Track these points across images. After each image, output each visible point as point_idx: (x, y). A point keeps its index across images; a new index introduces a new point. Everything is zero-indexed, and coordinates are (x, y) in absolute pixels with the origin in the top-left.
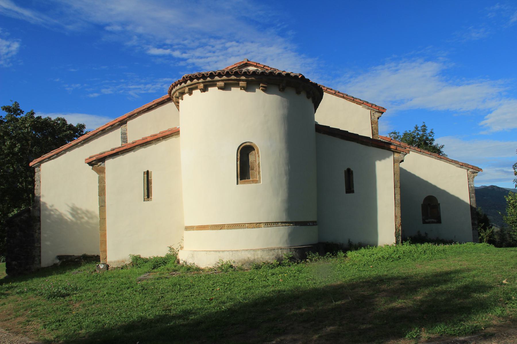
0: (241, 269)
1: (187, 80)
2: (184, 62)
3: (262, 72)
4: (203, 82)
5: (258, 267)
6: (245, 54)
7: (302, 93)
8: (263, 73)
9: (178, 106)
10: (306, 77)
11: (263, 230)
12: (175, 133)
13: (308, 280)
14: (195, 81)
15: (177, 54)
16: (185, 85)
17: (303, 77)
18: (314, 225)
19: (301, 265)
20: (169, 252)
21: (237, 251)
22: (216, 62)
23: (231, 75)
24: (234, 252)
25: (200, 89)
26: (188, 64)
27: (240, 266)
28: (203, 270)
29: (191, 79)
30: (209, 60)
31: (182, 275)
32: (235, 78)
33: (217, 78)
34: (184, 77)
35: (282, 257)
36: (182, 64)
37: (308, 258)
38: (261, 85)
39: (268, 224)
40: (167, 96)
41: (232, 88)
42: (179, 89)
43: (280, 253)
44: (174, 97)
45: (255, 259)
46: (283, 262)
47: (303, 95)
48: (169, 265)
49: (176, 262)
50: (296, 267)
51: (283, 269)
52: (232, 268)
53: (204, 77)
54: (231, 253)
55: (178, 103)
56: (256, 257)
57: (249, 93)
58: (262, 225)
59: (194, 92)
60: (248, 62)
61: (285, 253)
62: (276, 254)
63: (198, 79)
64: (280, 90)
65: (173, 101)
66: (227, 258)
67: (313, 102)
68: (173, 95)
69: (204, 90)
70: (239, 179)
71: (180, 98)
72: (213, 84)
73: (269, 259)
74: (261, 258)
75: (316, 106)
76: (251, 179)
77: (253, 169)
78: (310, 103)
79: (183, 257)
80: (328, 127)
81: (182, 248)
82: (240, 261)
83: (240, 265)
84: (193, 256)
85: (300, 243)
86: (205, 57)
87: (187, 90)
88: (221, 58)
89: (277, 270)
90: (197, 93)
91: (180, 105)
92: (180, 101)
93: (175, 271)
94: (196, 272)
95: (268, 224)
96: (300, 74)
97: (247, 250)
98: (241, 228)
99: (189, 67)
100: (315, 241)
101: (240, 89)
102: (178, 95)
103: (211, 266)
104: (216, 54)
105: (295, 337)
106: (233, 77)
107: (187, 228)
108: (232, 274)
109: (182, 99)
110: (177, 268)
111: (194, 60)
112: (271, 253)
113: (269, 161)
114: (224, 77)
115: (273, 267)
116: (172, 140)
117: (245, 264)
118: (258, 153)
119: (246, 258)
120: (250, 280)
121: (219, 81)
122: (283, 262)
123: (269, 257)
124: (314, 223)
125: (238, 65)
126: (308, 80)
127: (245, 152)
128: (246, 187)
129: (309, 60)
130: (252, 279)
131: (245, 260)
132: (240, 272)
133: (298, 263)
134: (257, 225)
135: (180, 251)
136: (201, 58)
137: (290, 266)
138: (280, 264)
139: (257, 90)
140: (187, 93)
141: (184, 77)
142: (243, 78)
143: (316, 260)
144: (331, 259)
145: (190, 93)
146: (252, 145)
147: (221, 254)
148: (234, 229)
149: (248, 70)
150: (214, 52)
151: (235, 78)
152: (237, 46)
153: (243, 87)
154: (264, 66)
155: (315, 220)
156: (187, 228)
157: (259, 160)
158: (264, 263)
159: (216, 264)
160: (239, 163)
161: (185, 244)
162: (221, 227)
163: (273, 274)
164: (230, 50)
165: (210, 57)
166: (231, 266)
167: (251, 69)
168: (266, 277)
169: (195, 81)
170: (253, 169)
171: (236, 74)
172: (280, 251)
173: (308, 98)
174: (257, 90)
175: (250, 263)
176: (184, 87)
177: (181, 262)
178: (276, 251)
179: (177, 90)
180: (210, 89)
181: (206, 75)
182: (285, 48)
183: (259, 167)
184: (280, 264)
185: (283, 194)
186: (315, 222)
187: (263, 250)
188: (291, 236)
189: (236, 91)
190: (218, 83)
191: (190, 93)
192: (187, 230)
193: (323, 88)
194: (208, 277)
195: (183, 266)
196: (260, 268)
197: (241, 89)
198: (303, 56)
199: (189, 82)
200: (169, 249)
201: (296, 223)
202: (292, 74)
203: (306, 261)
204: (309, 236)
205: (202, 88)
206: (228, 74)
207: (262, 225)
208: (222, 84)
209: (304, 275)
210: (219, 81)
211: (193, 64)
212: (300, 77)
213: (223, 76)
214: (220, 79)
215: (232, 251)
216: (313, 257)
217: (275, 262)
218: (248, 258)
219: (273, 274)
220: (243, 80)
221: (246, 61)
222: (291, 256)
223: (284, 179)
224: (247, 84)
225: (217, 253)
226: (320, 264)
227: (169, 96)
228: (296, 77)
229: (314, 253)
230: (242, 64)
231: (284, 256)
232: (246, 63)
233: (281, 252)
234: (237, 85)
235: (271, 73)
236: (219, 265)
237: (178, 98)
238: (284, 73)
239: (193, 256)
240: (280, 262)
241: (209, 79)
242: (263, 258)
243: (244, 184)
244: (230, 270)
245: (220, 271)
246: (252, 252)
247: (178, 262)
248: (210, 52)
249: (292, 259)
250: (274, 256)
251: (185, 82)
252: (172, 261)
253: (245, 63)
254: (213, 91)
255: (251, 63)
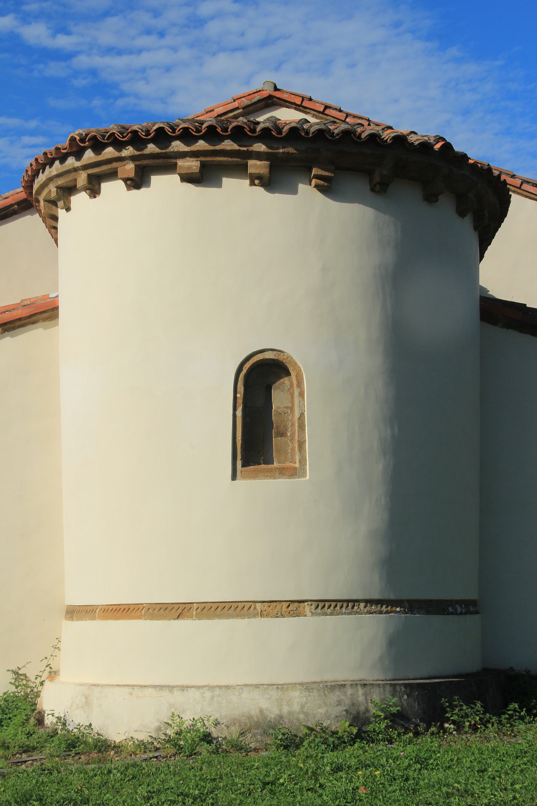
0: (239, 748)
1: (84, 149)
2: (63, 64)
3: (320, 132)
4: (133, 158)
5: (290, 743)
6: (264, 44)
7: (442, 198)
8: (321, 133)
9: (53, 229)
10: (457, 148)
11: (310, 623)
12: (45, 313)
13: (448, 795)
14: (110, 152)
15: (36, 33)
16: (78, 164)
17: (448, 146)
18: (468, 613)
19: (428, 741)
20: (13, 689)
21: (227, 687)
22: (168, 69)
23: (222, 139)
24: (217, 692)
25: (125, 180)
26: (77, 74)
27: (235, 736)
28: (117, 748)
29: (98, 145)
30: (145, 59)
31: (49, 765)
32: (236, 147)
33: (177, 146)
34: (73, 139)
35: (367, 710)
36: (54, 69)
37: (447, 720)
38: (315, 171)
39: (324, 605)
40: (17, 193)
41: (226, 181)
42: (59, 176)
43: (361, 699)
44: (41, 198)
45: (281, 717)
46: (370, 728)
47: (446, 206)
48: (11, 730)
49: (32, 721)
50: (409, 748)
51: (372, 751)
52: (210, 742)
53: (136, 139)
54: (208, 694)
55: (55, 218)
56: (285, 709)
57: (277, 195)
58: (307, 608)
59: (106, 187)
60: (277, 94)
61: (376, 698)
62: (348, 702)
63: (119, 145)
64: (373, 190)
65: (39, 211)
66: (194, 711)
67: (476, 228)
68: (39, 192)
69: (137, 182)
70: (239, 463)
71: (60, 203)
72: (166, 165)
73: (327, 716)
74: (302, 711)
75: (485, 240)
76: (276, 464)
77: (282, 434)
78: (465, 229)
79: (57, 703)
80: (522, 307)
81: (53, 674)
82: (234, 722)
83: (234, 732)
84: (87, 703)
85: (426, 667)
86: (130, 52)
87: (82, 179)
88: (185, 54)
89: (350, 754)
90: (113, 189)
91: (61, 225)
92: (61, 213)
93: (27, 749)
94: (94, 755)
95: (324, 605)
96: (440, 139)
97: (257, 686)
98: (242, 616)
99: (81, 82)
100: (471, 664)
101: (248, 182)
102: (53, 194)
103: (143, 736)
104: (168, 40)
105: (292, 464)
106: (228, 145)
107: (74, 612)
108: (209, 763)
109: (68, 209)
110: (33, 742)
111: (98, 61)
112: (333, 697)
113: (332, 410)
114: (201, 145)
115: (338, 742)
116: (32, 337)
117: (249, 730)
118: (300, 384)
119: (255, 712)
120: (265, 784)
121: (183, 155)
122: (370, 728)
123: (326, 712)
124: (469, 607)
125: (245, 102)
126: (464, 157)
127: (261, 381)
128: (260, 488)
129: (471, 69)
130: (273, 783)
131: (250, 717)
132: (235, 756)
133: (417, 734)
134: (293, 607)
135: (47, 683)
136: (120, 52)
137: (390, 742)
138: (359, 736)
139: (302, 187)
140: (85, 189)
141: (73, 139)
142: (260, 147)
143: (474, 728)
144: (522, 727)
145: (94, 191)
146: (281, 358)
147: (178, 697)
148: (220, 617)
149: (275, 121)
150: (162, 34)
151: (236, 147)
152: (237, 15)
153: (259, 177)
154: (327, 107)
155: (473, 596)
156: (74, 612)
157: (302, 407)
158: (311, 729)
159: (159, 729)
160: (239, 413)
161: (65, 663)
162: (179, 611)
163: (338, 769)
164: (213, 29)
165: (148, 50)
166: (207, 738)
167: (287, 116)
168: (315, 775)
169: (110, 152)
170: (282, 434)
171: (238, 134)
172: (361, 691)
173: (461, 213)
174: (302, 187)
175: (267, 727)
176: (75, 170)
177: (49, 720)
178: (349, 691)
179: (50, 180)
180: (156, 180)
181: (142, 134)
182: (397, 25)
183: (302, 427)
184: (359, 736)
185: (371, 514)
186: (474, 603)
187: (307, 687)
188: (397, 646)
189: (234, 187)
190: (180, 163)
191: (94, 191)
192: (71, 618)
193: (509, 180)
194: (134, 773)
195: (55, 733)
196: (297, 747)
197: (252, 184)
198: (454, 51)
199: (89, 156)
200: (10, 677)
201: (412, 606)
202: (412, 139)
203: (442, 727)
204: (451, 648)
205: (132, 175)
206: (212, 134)
207: (307, 608)
208: (191, 165)
209: (436, 775)
210: (183, 155)
211: (93, 72)
212: (437, 147)
213: (196, 139)
214: (186, 149)
215: (211, 688)
216: (467, 716)
217: (343, 726)
218: (261, 711)
219: (338, 769)
220: (259, 156)
221: (269, 91)
222: (394, 710)
223: (378, 468)
224: (271, 167)
225: (165, 693)
226: (488, 739)
227: (23, 196)
228: (426, 146)
229: (470, 702)
230: (257, 97)
231: (373, 711)
232: (270, 97)
233: (365, 695)
234: (238, 169)
235: (347, 134)
236: (171, 732)
237: (54, 203)
238: (387, 135)
239: (87, 703)
240: (362, 728)
241: (151, 148)
242: (306, 714)
243: (255, 477)
244: (204, 749)
245: (173, 751)
246: (274, 694)
247: (40, 722)
248: (148, 32)
249: (398, 719)
250: (341, 708)
251: (78, 154)
252: (17, 720)
253: (265, 94)
254: (165, 186)
255: (285, 96)
